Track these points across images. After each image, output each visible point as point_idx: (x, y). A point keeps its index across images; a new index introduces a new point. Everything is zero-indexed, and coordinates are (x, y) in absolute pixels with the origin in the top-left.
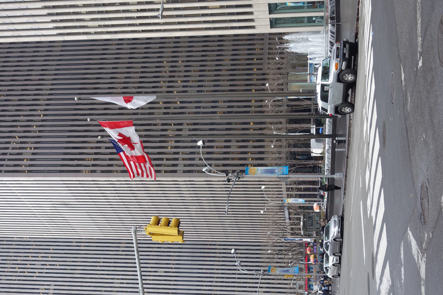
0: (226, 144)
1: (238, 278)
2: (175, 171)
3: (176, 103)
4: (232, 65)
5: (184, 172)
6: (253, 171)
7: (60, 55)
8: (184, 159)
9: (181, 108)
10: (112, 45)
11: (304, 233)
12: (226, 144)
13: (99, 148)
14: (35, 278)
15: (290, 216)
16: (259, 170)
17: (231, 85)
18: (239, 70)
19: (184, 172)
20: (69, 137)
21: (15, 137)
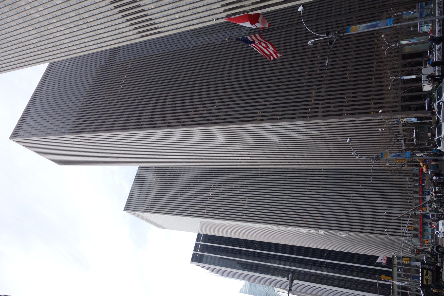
0: (353, 95)
1: (368, 194)
2: (317, 116)
3: (317, 71)
4: (357, 40)
5: (323, 116)
6: (354, 29)
7: (242, 51)
8: (323, 108)
9: (320, 74)
10: (273, 39)
11: (416, 143)
12: (353, 95)
13: (266, 105)
14: (237, 194)
15: (406, 143)
16: (361, 27)
17: (356, 54)
18: (363, 43)
19: (323, 116)
20: (247, 100)
21: (215, 103)
